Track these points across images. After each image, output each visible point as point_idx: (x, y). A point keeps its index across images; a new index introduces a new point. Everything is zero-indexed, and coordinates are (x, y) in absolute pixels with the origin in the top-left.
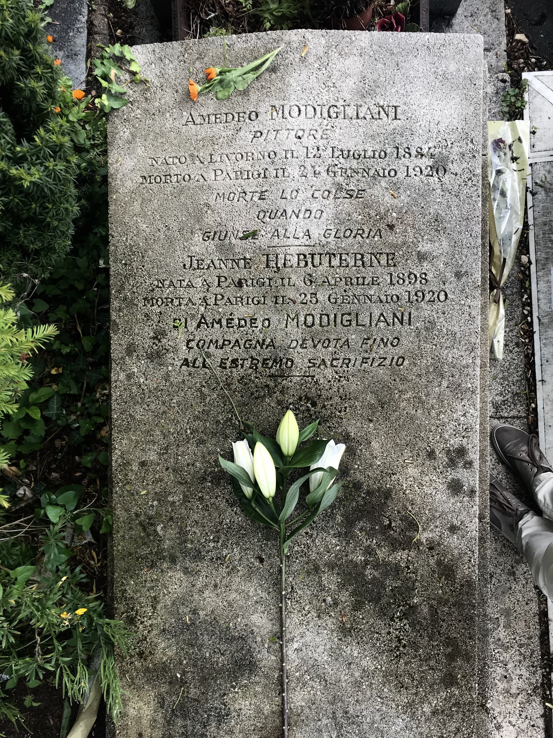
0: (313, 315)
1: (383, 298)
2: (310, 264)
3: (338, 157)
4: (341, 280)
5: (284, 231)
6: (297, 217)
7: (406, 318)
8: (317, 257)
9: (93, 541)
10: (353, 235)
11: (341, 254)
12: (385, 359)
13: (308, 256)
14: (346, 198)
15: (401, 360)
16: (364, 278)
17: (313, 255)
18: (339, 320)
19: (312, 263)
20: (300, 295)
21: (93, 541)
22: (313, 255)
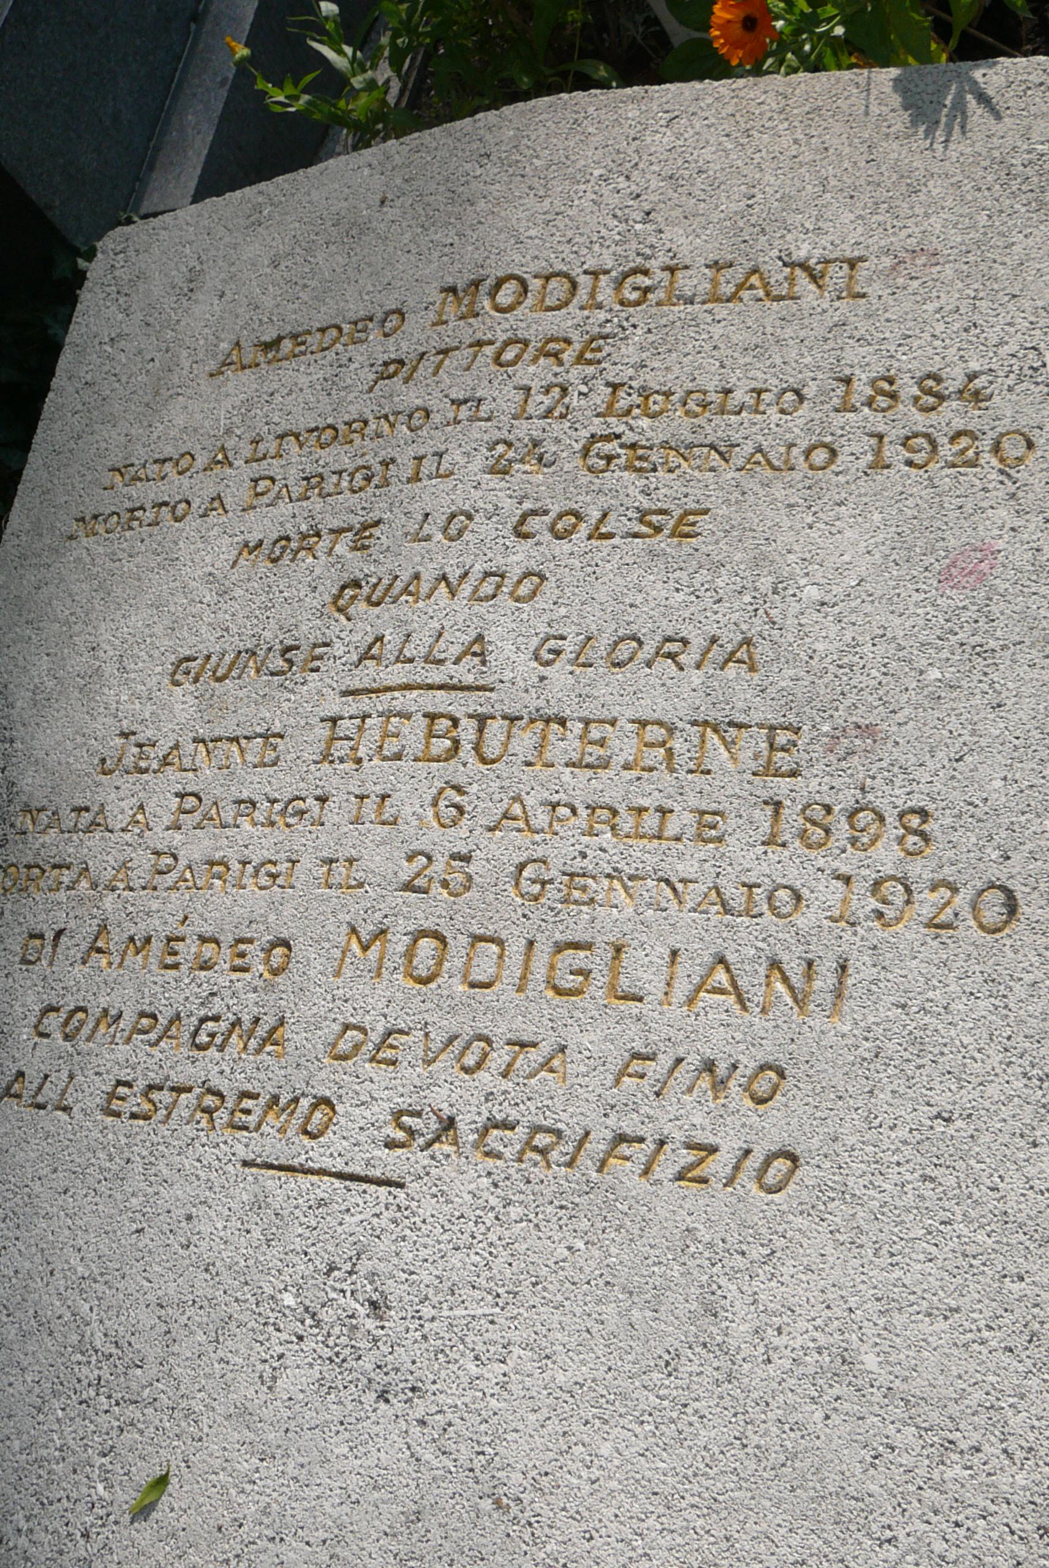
0: (442, 940)
1: (736, 896)
2: (466, 751)
3: (628, 412)
4: (574, 811)
5: (399, 639)
6: (453, 593)
7: (825, 981)
8: (495, 727)
9: (237, 56)
10: (642, 656)
11: (587, 722)
12: (713, 1150)
13: (464, 722)
14: (636, 535)
15: (782, 1164)
16: (664, 812)
17: (482, 721)
18: (539, 970)
19: (477, 748)
20: (131, 528)
21: (237, 56)
22: (482, 721)
